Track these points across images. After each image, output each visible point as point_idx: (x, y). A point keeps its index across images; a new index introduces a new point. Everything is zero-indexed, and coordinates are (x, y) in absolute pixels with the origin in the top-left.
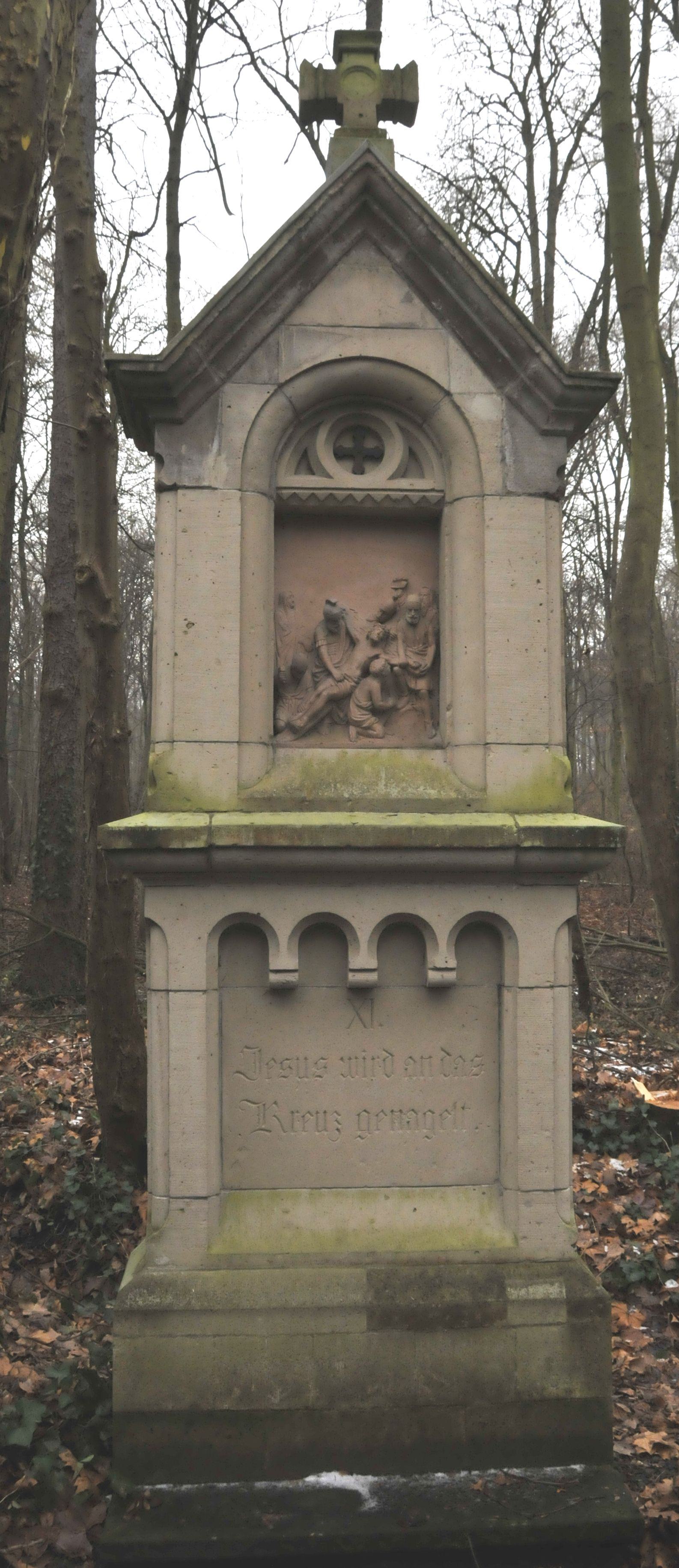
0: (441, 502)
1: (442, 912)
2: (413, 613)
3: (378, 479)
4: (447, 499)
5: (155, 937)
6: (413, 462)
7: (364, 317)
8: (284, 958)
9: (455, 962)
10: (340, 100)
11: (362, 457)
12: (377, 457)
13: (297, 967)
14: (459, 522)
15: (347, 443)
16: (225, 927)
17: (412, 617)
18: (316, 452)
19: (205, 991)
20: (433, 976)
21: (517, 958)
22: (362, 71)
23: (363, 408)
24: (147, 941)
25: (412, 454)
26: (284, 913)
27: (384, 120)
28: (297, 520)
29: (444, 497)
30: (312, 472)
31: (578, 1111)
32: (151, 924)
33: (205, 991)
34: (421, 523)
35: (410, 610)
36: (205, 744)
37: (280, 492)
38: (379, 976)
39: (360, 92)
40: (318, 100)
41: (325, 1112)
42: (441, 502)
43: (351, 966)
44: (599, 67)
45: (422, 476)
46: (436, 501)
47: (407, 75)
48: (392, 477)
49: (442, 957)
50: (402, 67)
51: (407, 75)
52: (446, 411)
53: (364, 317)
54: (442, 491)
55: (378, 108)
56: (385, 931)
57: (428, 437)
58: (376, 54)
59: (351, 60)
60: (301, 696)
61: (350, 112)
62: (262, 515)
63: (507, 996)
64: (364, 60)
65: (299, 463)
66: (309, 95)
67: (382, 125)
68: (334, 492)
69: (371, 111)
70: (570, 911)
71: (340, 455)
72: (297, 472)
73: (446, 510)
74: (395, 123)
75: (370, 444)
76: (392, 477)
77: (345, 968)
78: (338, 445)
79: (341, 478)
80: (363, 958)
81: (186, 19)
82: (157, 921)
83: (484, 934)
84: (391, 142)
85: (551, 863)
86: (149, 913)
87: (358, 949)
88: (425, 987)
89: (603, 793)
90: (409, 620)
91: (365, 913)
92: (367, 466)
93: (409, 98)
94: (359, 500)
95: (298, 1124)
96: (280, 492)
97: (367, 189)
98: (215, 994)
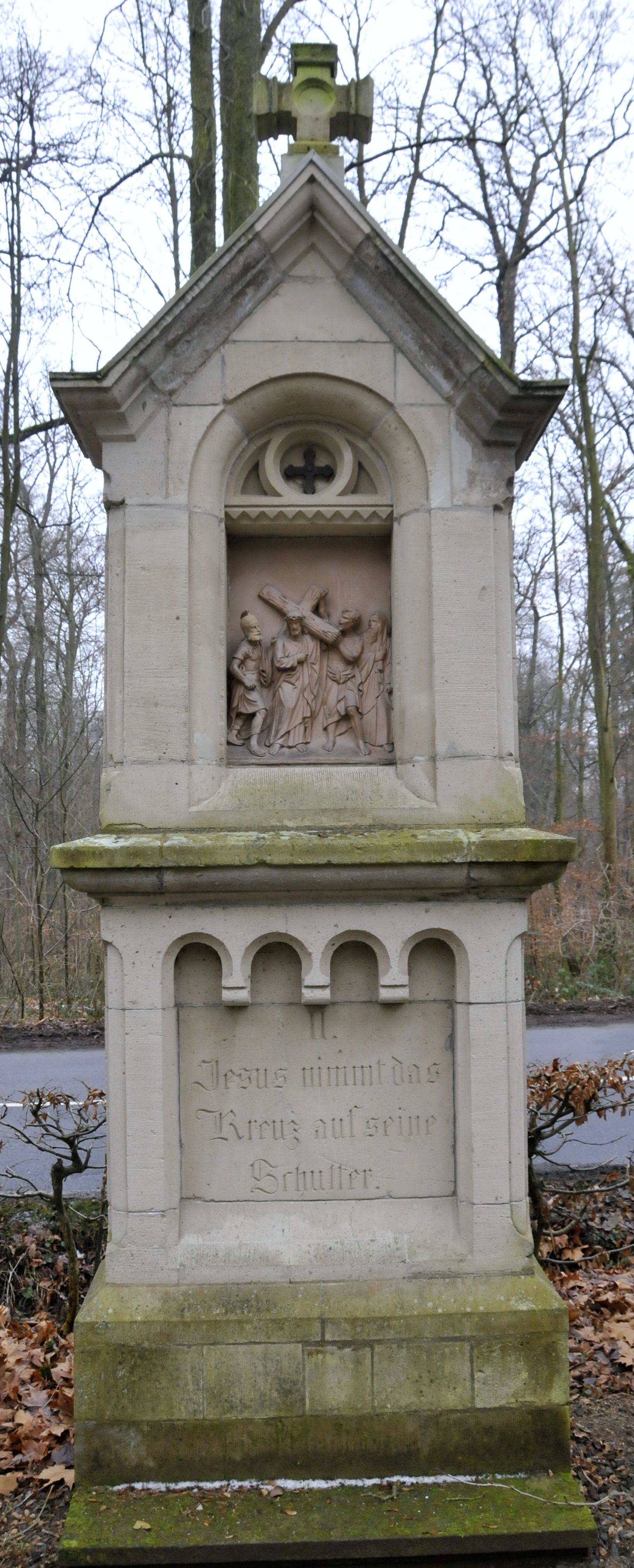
1: (394, 928)
3: (330, 498)
4: (395, 515)
6: (362, 479)
10: (294, 114)
11: (309, 472)
12: (328, 475)
15: (298, 462)
19: (470, 1004)
22: (317, 87)
23: (305, 430)
25: (360, 467)
26: (236, 932)
28: (245, 544)
29: (392, 512)
30: (265, 493)
31: (534, 1191)
32: (106, 943)
33: (470, 1004)
34: (374, 544)
37: (229, 510)
42: (390, 517)
43: (307, 982)
45: (374, 490)
47: (362, 87)
48: (342, 494)
51: (362, 87)
54: (392, 506)
56: (336, 953)
58: (332, 68)
59: (305, 74)
61: (303, 128)
62: (213, 546)
63: (459, 1009)
64: (322, 74)
71: (289, 474)
72: (244, 491)
73: (396, 526)
75: (321, 461)
76: (342, 494)
77: (219, 988)
78: (286, 465)
79: (290, 498)
80: (316, 974)
81: (184, 281)
83: (435, 949)
86: (106, 936)
87: (389, 967)
91: (315, 930)
92: (319, 485)
94: (347, 516)
95: (255, 1134)
96: (229, 510)
97: (313, 207)
98: (173, 1013)
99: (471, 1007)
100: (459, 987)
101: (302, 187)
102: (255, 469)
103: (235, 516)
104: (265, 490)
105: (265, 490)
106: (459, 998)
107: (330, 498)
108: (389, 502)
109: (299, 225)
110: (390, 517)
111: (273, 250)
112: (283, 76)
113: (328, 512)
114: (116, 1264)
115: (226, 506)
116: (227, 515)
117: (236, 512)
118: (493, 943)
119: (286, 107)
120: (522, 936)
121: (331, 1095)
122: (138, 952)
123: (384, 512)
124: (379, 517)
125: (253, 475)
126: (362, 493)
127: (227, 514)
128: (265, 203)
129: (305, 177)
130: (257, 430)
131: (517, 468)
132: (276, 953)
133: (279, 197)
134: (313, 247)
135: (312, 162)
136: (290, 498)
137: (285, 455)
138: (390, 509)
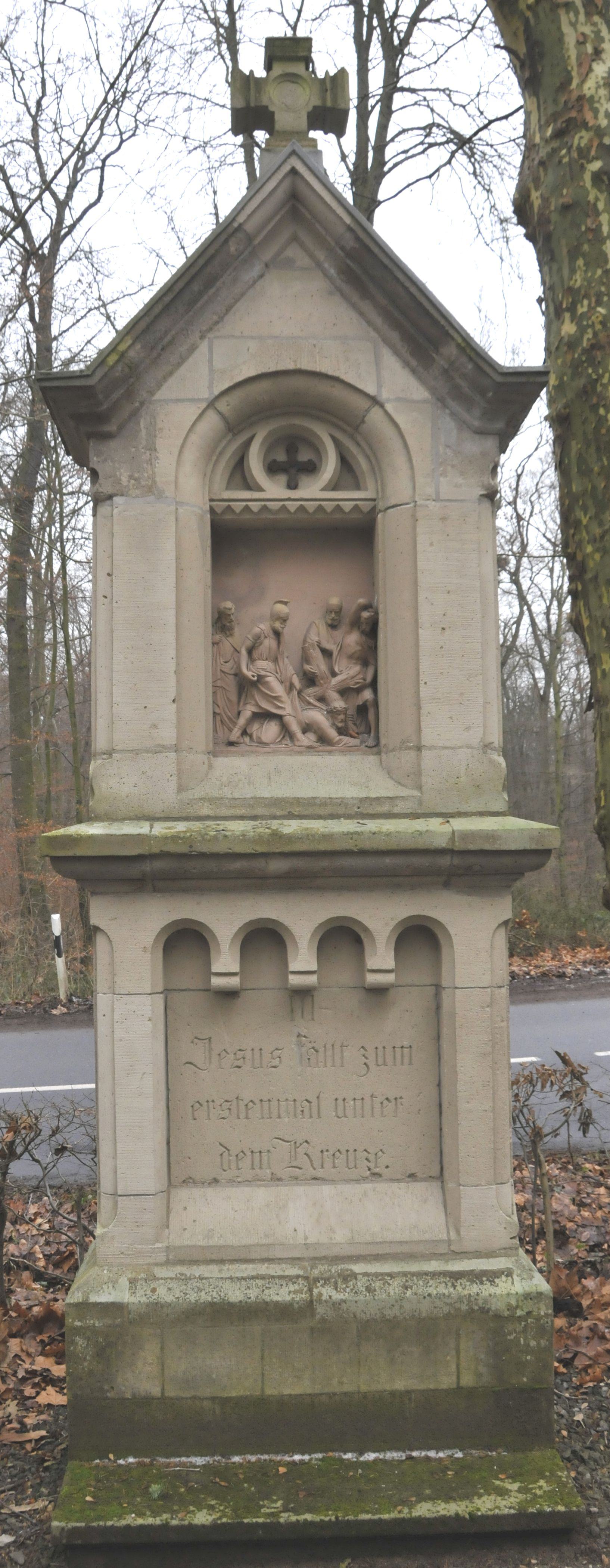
0: (373, 511)
1: (380, 916)
2: (333, 615)
3: (313, 490)
4: (381, 505)
5: (100, 940)
7: (289, 323)
8: (226, 961)
9: (238, 966)
11: (292, 465)
12: (311, 468)
13: (314, 967)
14: (389, 528)
15: (281, 457)
16: (319, 938)
17: (333, 619)
18: (250, 470)
19: (456, 988)
20: (295, 980)
21: (453, 961)
23: (291, 418)
24: (445, 951)
25: (345, 463)
26: (225, 919)
27: (315, 130)
28: (233, 541)
32: (97, 929)
33: (456, 988)
34: (353, 537)
35: (331, 612)
36: (151, 757)
38: (241, 979)
39: (290, 104)
40: (250, 113)
41: (344, 1100)
42: (373, 509)
43: (214, 969)
44: (493, 20)
45: (358, 487)
46: (368, 509)
48: (324, 489)
49: (381, 958)
50: (332, 74)
52: (375, 416)
53: (289, 323)
54: (374, 500)
55: (310, 115)
57: (358, 444)
59: (279, 69)
60: (239, 709)
64: (298, 68)
65: (232, 475)
66: (241, 104)
67: (312, 134)
68: (267, 503)
69: (304, 122)
70: (508, 915)
71: (272, 469)
74: (326, 133)
75: (304, 456)
77: (209, 973)
78: (271, 458)
80: (303, 959)
82: (101, 927)
83: (420, 938)
84: (320, 152)
85: (475, 869)
87: (219, 951)
88: (287, 989)
89: (552, 799)
90: (330, 622)
91: (302, 919)
92: (304, 480)
93: (342, 106)
98: (160, 1000)
99: (457, 990)
100: (444, 973)
101: (284, 177)
102: (240, 465)
103: (219, 511)
104: (248, 484)
105: (248, 484)
106: (444, 983)
107: (313, 490)
108: (374, 497)
109: (282, 212)
110: (373, 509)
111: (256, 242)
112: (260, 73)
113: (311, 506)
114: (111, 1234)
115: (211, 500)
116: (212, 510)
117: (220, 506)
118: (475, 934)
119: (265, 101)
120: (506, 923)
121: (326, 1072)
122: (130, 933)
123: (366, 506)
124: (361, 512)
125: (239, 473)
126: (341, 490)
127: (211, 507)
128: (227, 218)
129: (286, 168)
130: (237, 426)
131: (503, 450)
132: (265, 939)
133: (243, 208)
134: (295, 238)
135: (294, 153)
136: (274, 490)
137: (269, 447)
138: (372, 503)
